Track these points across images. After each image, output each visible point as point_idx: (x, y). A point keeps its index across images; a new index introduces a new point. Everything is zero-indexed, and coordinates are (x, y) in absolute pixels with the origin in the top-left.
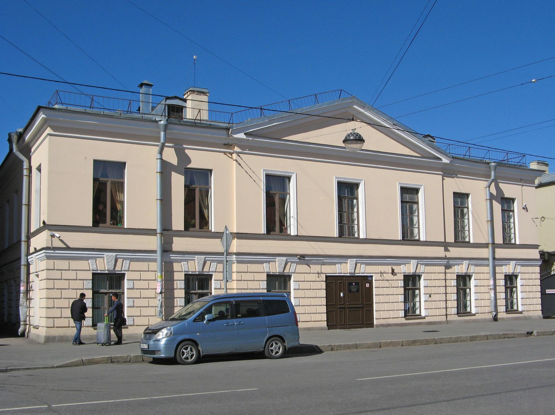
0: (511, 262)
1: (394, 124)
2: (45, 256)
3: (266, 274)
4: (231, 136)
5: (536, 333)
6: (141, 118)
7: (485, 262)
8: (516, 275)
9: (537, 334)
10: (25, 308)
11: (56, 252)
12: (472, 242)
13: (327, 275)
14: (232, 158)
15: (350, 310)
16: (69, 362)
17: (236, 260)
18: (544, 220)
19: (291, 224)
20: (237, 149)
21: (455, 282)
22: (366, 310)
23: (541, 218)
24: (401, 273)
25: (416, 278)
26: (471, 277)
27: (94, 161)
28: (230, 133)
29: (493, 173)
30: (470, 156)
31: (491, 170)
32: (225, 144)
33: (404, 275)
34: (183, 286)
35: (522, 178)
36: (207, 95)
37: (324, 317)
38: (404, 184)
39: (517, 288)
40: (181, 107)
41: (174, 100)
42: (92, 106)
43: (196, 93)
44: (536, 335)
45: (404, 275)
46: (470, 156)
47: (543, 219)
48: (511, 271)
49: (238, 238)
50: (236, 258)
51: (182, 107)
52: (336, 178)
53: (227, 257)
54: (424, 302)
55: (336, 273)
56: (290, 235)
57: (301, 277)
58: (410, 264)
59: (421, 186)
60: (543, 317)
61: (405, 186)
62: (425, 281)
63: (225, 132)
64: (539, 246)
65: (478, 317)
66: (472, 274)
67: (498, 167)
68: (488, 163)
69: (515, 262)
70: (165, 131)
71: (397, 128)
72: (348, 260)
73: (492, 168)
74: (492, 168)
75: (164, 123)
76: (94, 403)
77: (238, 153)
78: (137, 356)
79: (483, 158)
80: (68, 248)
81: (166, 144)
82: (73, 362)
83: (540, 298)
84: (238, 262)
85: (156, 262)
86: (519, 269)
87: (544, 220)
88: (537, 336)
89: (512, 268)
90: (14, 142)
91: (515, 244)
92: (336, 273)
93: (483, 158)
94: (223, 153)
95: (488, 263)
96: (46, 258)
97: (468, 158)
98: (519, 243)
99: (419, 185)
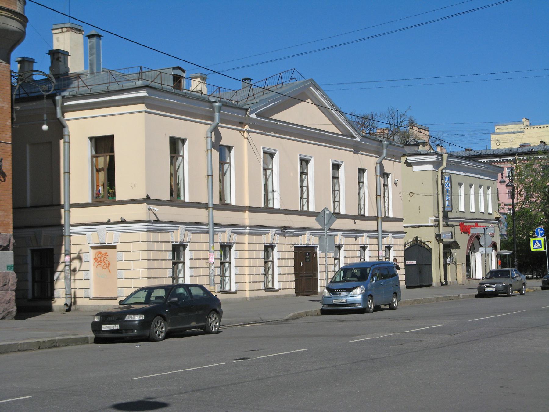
0: (228, 228)
1: (332, 105)
2: (147, 229)
3: (263, 245)
4: (248, 116)
5: (462, 296)
6: (199, 98)
7: (204, 228)
8: (230, 245)
9: (463, 296)
10: (69, 280)
11: (154, 224)
12: (367, 215)
13: (295, 245)
14: (243, 136)
15: (307, 279)
16: (291, 314)
17: (249, 232)
18: (412, 196)
19: (274, 198)
20: (247, 127)
21: (218, 254)
22: (306, 279)
23: (409, 193)
24: (169, 242)
25: (180, 248)
26: (340, 248)
27: (170, 137)
28: (248, 113)
29: (385, 151)
30: (162, 84)
31: (383, 148)
32: (240, 123)
33: (172, 245)
34: (293, 257)
35: (394, 155)
36: (82, 34)
37: (293, 285)
38: (303, 156)
39: (340, 260)
40: (176, 77)
41: (176, 70)
42: (140, 77)
43: (74, 31)
44: (462, 298)
45: (172, 245)
46: (162, 84)
47: (411, 194)
48: (226, 241)
49: (250, 211)
50: (250, 230)
51: (179, 77)
52: (332, 160)
53: (377, 235)
54: (189, 278)
55: (299, 244)
56: (183, 201)
57: (348, 247)
58: (177, 231)
59: (312, 157)
60: (406, 287)
61: (303, 158)
62: (370, 251)
63: (244, 112)
64: (404, 219)
65: (281, 292)
66: (342, 245)
67: (389, 145)
68: (381, 141)
69: (184, 227)
70: (387, 148)
71: (333, 108)
72: (306, 232)
73: (216, 109)
74: (216, 109)
75: (387, 143)
76: (149, 375)
77: (248, 132)
78: (306, 312)
79: (230, 100)
80: (158, 221)
81: (220, 124)
82: (177, 329)
83: (404, 269)
84: (250, 234)
85: (208, 234)
86: (190, 237)
87: (412, 196)
88: (463, 298)
89: (307, 238)
90: (59, 107)
91: (308, 211)
92: (299, 244)
93: (152, 82)
94: (238, 131)
95: (208, 229)
96: (146, 231)
97: (169, 89)
98: (189, 201)
99: (341, 162)
